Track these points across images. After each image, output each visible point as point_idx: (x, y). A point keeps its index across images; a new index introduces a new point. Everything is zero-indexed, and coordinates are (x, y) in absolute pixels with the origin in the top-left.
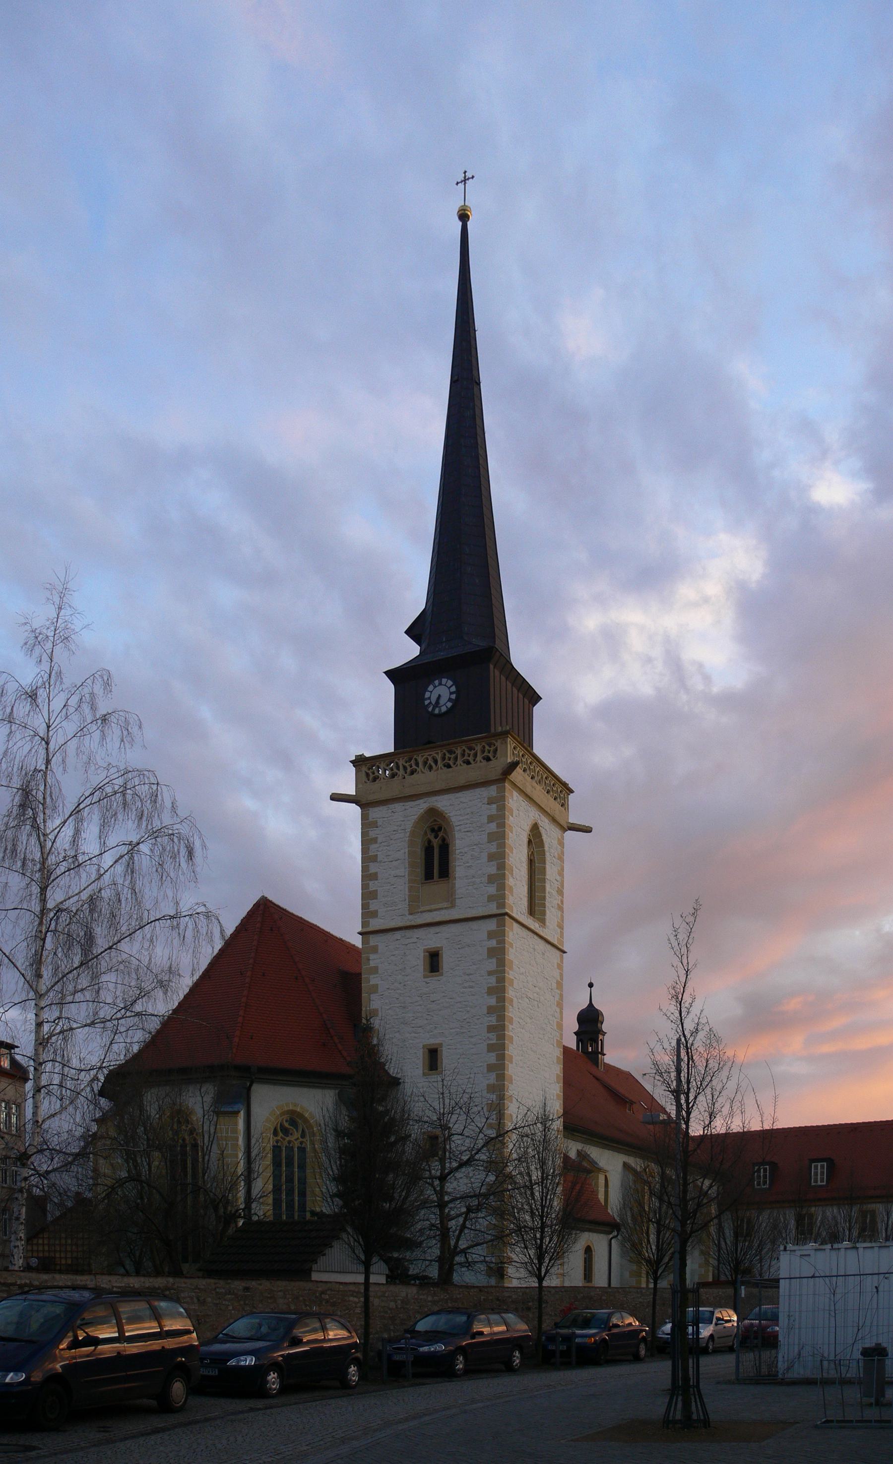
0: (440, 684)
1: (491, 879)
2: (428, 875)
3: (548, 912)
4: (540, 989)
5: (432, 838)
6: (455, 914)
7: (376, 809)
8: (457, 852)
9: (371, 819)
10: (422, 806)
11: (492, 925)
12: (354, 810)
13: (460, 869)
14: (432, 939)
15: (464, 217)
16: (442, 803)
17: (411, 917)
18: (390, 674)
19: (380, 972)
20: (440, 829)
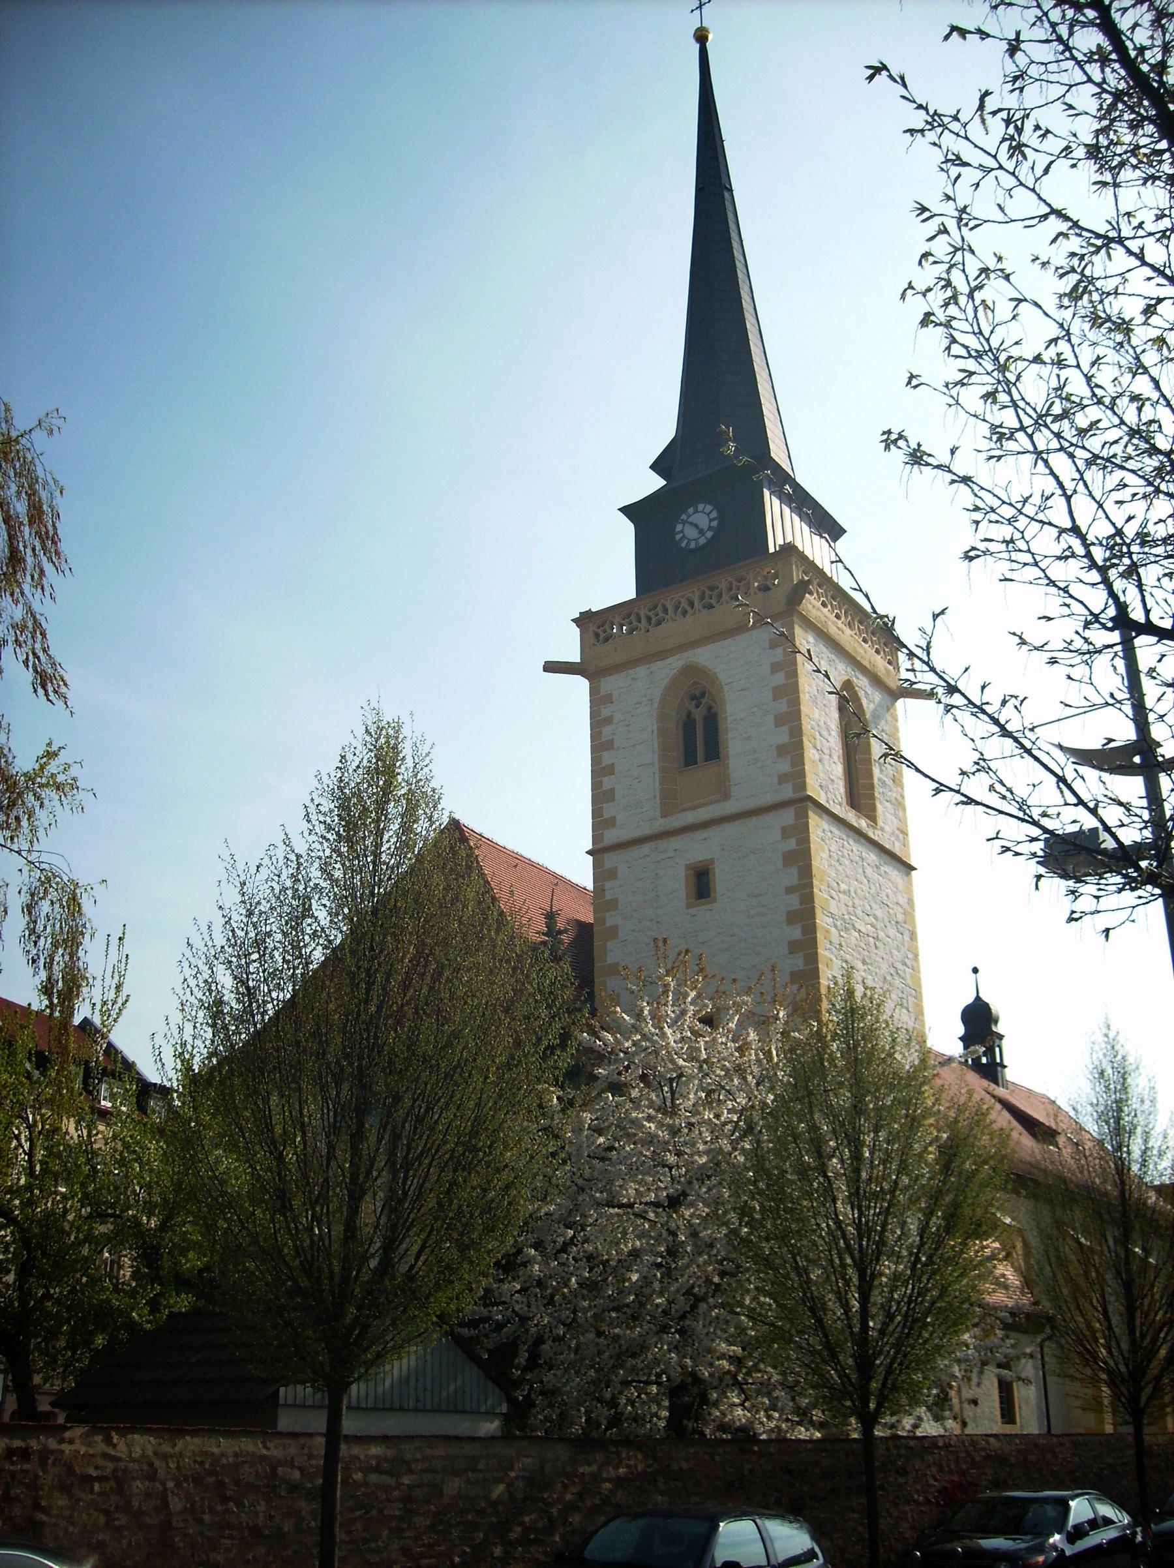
0: (696, 511)
1: (782, 750)
2: (690, 759)
3: (879, 806)
4: (876, 918)
5: (691, 706)
6: (728, 807)
7: (612, 678)
8: (729, 719)
9: (602, 693)
10: (675, 663)
11: (787, 817)
12: (581, 685)
13: (734, 745)
14: (695, 850)
15: (701, 37)
16: (703, 656)
17: (662, 821)
18: (627, 511)
19: (620, 906)
20: (703, 695)
